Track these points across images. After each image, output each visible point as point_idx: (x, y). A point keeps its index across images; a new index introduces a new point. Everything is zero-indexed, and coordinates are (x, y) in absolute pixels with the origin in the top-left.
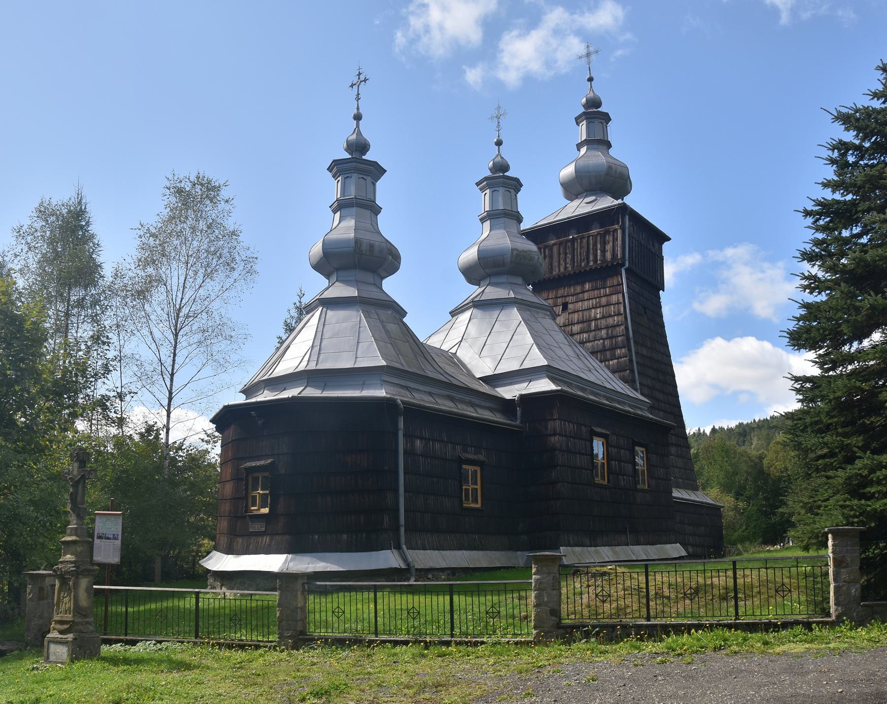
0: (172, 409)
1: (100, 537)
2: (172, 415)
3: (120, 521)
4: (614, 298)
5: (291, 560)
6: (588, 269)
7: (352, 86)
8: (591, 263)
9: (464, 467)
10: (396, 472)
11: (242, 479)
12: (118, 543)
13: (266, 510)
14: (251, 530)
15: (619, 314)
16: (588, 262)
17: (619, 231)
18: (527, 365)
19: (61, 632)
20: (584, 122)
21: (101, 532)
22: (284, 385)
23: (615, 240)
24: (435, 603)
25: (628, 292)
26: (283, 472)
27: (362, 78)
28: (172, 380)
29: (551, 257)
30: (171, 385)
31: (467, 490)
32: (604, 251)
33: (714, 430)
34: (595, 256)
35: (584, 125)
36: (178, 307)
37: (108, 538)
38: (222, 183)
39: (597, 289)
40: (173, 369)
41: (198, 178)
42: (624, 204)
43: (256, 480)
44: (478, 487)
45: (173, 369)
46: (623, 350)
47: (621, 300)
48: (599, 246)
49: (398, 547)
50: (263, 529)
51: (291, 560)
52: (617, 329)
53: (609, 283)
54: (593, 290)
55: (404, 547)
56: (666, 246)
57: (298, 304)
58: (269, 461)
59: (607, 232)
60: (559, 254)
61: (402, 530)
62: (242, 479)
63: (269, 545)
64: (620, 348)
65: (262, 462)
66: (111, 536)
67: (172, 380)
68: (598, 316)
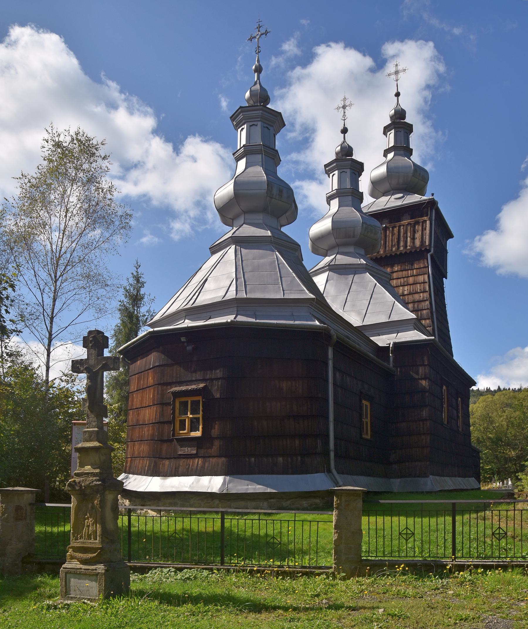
0: (51, 349)
2: (51, 355)
4: (421, 278)
5: (230, 482)
6: (398, 253)
7: (251, 39)
8: (402, 248)
10: (327, 400)
11: (169, 404)
13: (198, 434)
14: (180, 453)
15: (425, 291)
16: (399, 247)
17: (428, 222)
18: (395, 317)
19: (84, 562)
22: (209, 314)
25: (433, 274)
26: (218, 396)
27: (263, 30)
28: (51, 323)
30: (51, 327)
32: (413, 239)
35: (392, 134)
36: (58, 256)
38: (100, 142)
39: (405, 270)
40: (53, 313)
41: (77, 134)
42: (433, 198)
43: (184, 405)
45: (53, 313)
46: (428, 321)
47: (427, 280)
48: (409, 234)
49: (329, 471)
50: (194, 452)
52: (423, 303)
53: (416, 266)
54: (402, 271)
55: (334, 471)
56: (450, 242)
57: (135, 274)
58: (202, 385)
59: (417, 223)
61: (332, 455)
62: (169, 404)
63: (203, 467)
64: (425, 319)
65: (194, 387)
67: (51, 323)
68: (406, 293)
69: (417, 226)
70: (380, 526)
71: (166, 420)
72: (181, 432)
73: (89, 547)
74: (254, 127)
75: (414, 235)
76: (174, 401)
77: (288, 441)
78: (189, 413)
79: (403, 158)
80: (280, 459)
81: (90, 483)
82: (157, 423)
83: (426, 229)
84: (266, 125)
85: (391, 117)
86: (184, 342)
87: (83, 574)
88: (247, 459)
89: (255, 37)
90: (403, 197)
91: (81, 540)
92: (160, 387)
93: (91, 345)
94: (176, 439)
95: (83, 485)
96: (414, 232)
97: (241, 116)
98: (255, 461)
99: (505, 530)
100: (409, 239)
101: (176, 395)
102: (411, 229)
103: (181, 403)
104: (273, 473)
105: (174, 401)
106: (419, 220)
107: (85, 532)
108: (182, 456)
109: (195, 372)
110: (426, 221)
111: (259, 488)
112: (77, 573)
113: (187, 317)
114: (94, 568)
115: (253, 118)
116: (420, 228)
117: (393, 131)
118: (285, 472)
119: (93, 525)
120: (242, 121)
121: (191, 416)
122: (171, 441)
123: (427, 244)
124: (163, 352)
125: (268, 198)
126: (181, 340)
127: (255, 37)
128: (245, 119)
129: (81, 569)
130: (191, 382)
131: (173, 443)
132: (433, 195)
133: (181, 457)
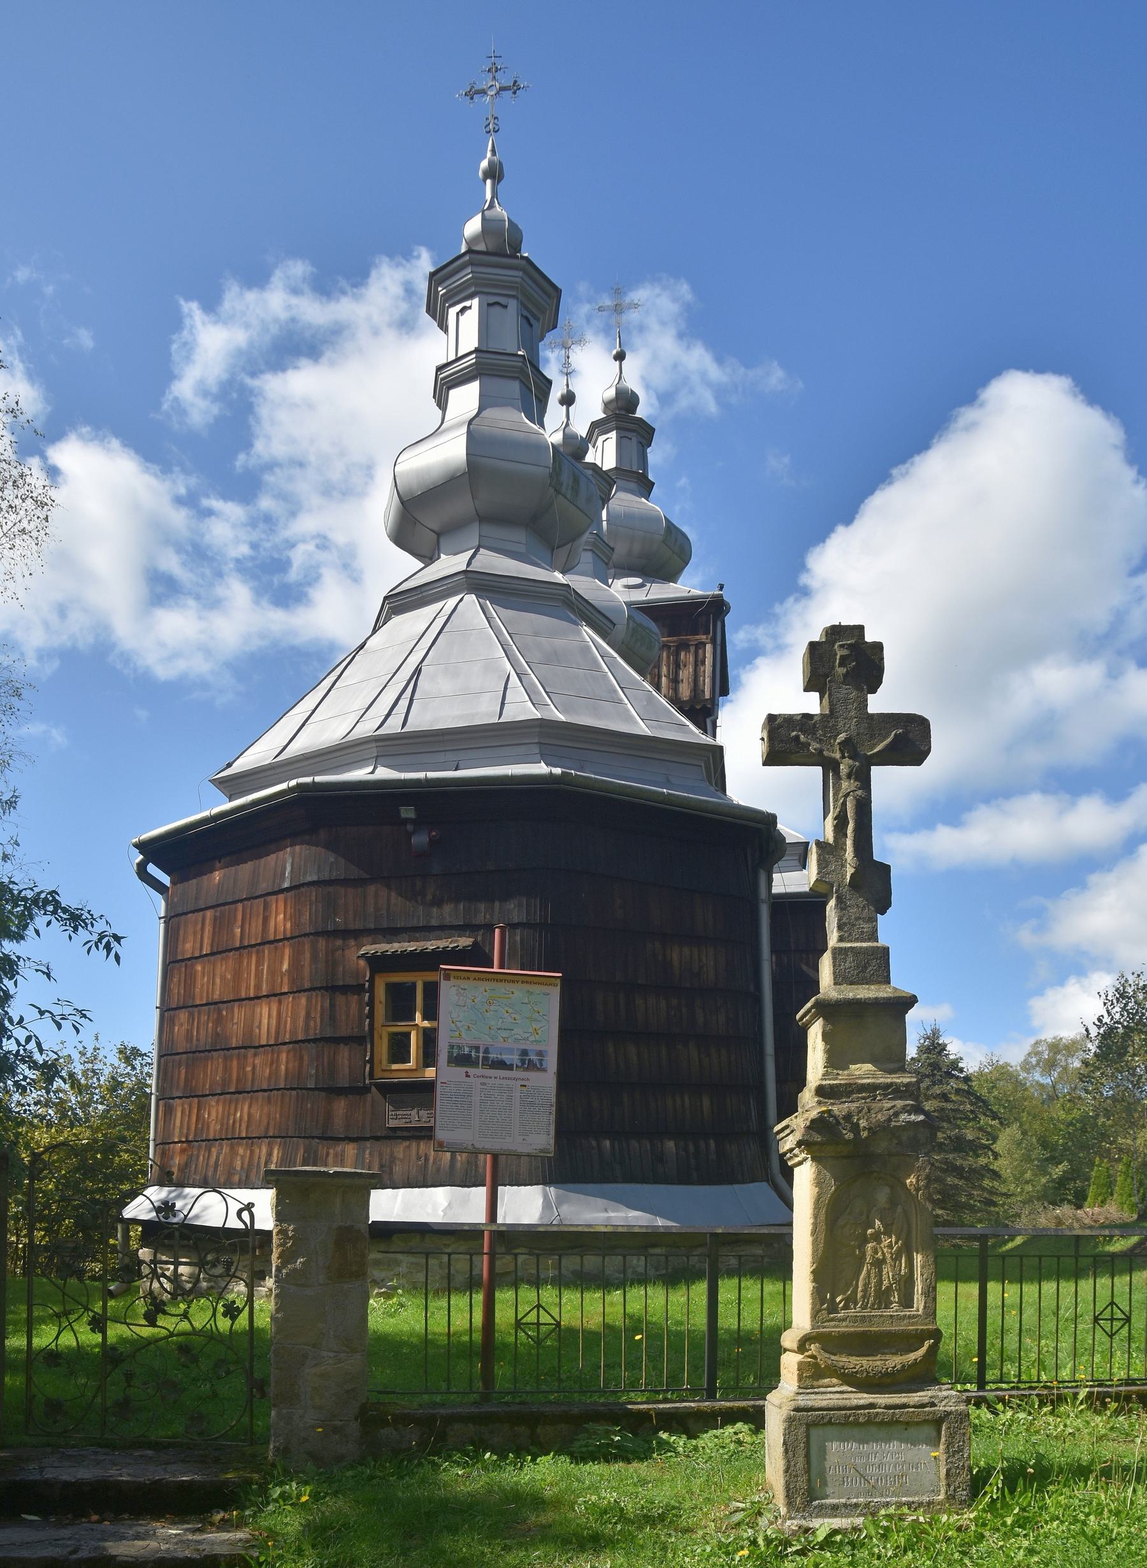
1: (461, 1060)
3: (555, 992)
11: (358, 989)
12: (547, 1081)
14: (393, 1123)
17: (709, 647)
20: (613, 434)
21: (467, 1039)
23: (699, 662)
24: (1067, 1301)
37: (501, 1065)
42: (721, 596)
48: (664, 670)
51: (560, 1202)
59: (684, 646)
66: (513, 1058)
69: (683, 654)
70: (1048, 1303)
71: (344, 1031)
72: (395, 1067)
73: (889, 1333)
74: (497, 309)
75: (677, 674)
76: (372, 980)
77: (687, 1099)
78: (418, 1016)
79: (638, 499)
80: (670, 1145)
81: (889, 1120)
82: (315, 1041)
83: (703, 663)
84: (526, 313)
85: (607, 405)
86: (406, 821)
87: (882, 1423)
88: (594, 1143)
89: (483, 92)
90: (641, 586)
91: (851, 1312)
92: (322, 943)
93: (841, 671)
94: (377, 1086)
95: (863, 1123)
96: (677, 666)
97: (467, 275)
98: (612, 1146)
99: (1097, 1327)
100: (664, 679)
101: (379, 963)
102: (668, 658)
103: (392, 988)
104: (656, 1181)
105: (372, 980)
106: (689, 640)
107: (866, 1285)
108: (399, 1133)
109: (438, 903)
110: (704, 644)
111: (634, 1217)
112: (856, 1424)
113: (380, 759)
114: (926, 1400)
115: (487, 285)
116: (692, 659)
117: (613, 434)
118: (683, 1177)
119: (897, 1258)
120: (469, 287)
121: (426, 1024)
122: (366, 1090)
123: (707, 695)
124: (330, 846)
125: (551, 490)
126: (399, 812)
127: (483, 92)
128: (476, 285)
129: (872, 1406)
130: (426, 931)
131: (369, 1097)
132: (721, 587)
133: (396, 1135)
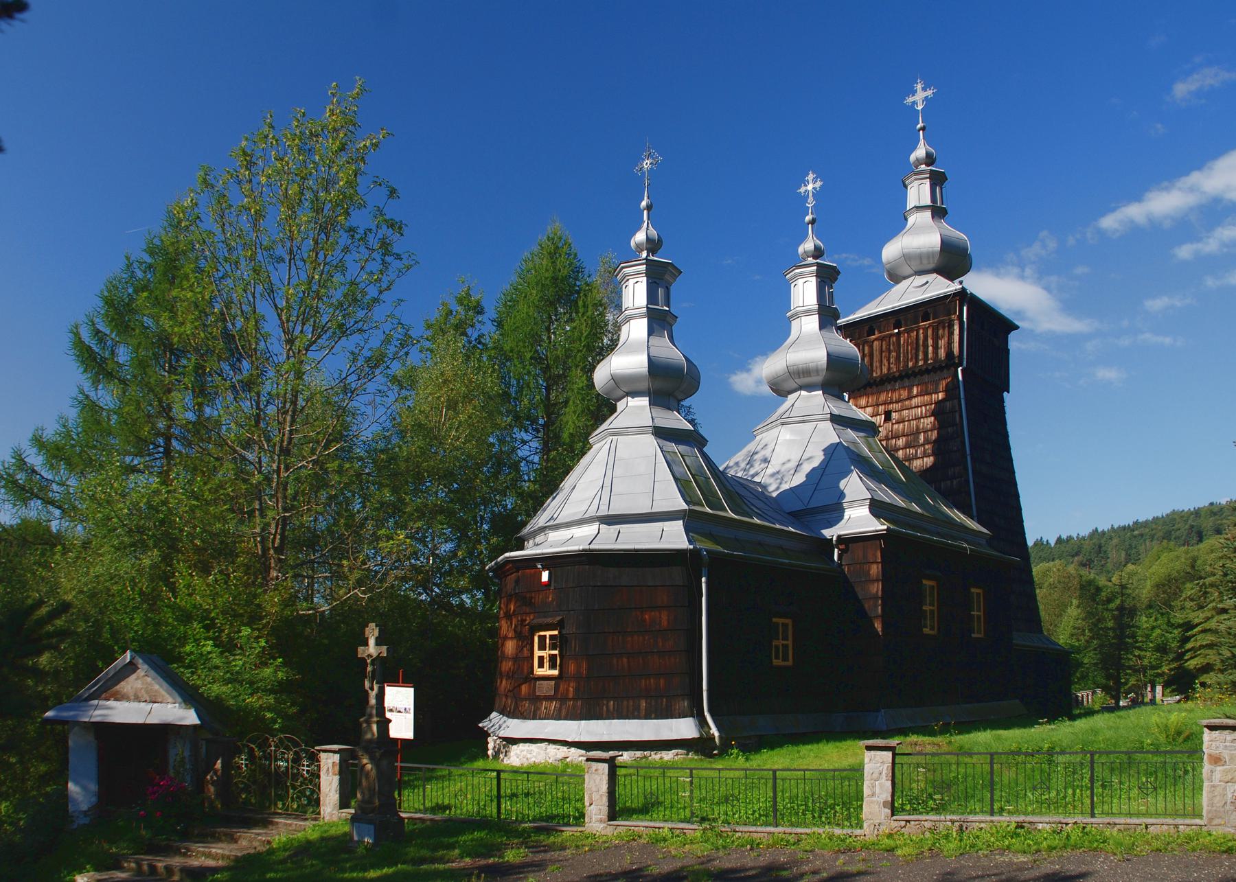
8: (921, 363)
9: (774, 620)
16: (917, 362)
23: (951, 334)
29: (871, 355)
31: (777, 647)
32: (936, 348)
33: (1059, 540)
34: (926, 353)
44: (790, 642)
56: (1012, 336)
60: (881, 351)
